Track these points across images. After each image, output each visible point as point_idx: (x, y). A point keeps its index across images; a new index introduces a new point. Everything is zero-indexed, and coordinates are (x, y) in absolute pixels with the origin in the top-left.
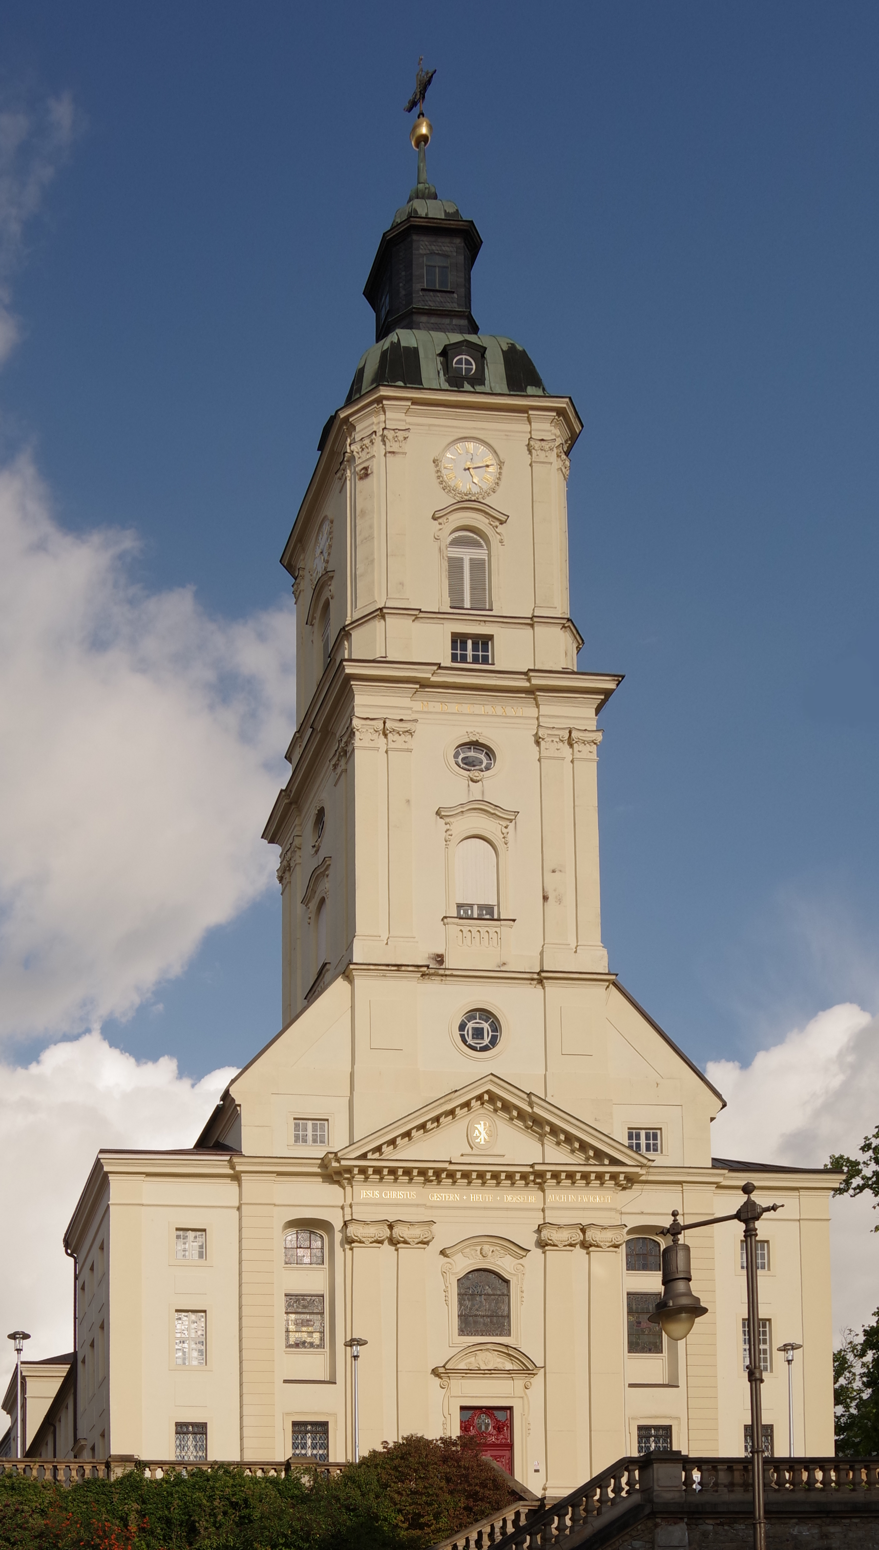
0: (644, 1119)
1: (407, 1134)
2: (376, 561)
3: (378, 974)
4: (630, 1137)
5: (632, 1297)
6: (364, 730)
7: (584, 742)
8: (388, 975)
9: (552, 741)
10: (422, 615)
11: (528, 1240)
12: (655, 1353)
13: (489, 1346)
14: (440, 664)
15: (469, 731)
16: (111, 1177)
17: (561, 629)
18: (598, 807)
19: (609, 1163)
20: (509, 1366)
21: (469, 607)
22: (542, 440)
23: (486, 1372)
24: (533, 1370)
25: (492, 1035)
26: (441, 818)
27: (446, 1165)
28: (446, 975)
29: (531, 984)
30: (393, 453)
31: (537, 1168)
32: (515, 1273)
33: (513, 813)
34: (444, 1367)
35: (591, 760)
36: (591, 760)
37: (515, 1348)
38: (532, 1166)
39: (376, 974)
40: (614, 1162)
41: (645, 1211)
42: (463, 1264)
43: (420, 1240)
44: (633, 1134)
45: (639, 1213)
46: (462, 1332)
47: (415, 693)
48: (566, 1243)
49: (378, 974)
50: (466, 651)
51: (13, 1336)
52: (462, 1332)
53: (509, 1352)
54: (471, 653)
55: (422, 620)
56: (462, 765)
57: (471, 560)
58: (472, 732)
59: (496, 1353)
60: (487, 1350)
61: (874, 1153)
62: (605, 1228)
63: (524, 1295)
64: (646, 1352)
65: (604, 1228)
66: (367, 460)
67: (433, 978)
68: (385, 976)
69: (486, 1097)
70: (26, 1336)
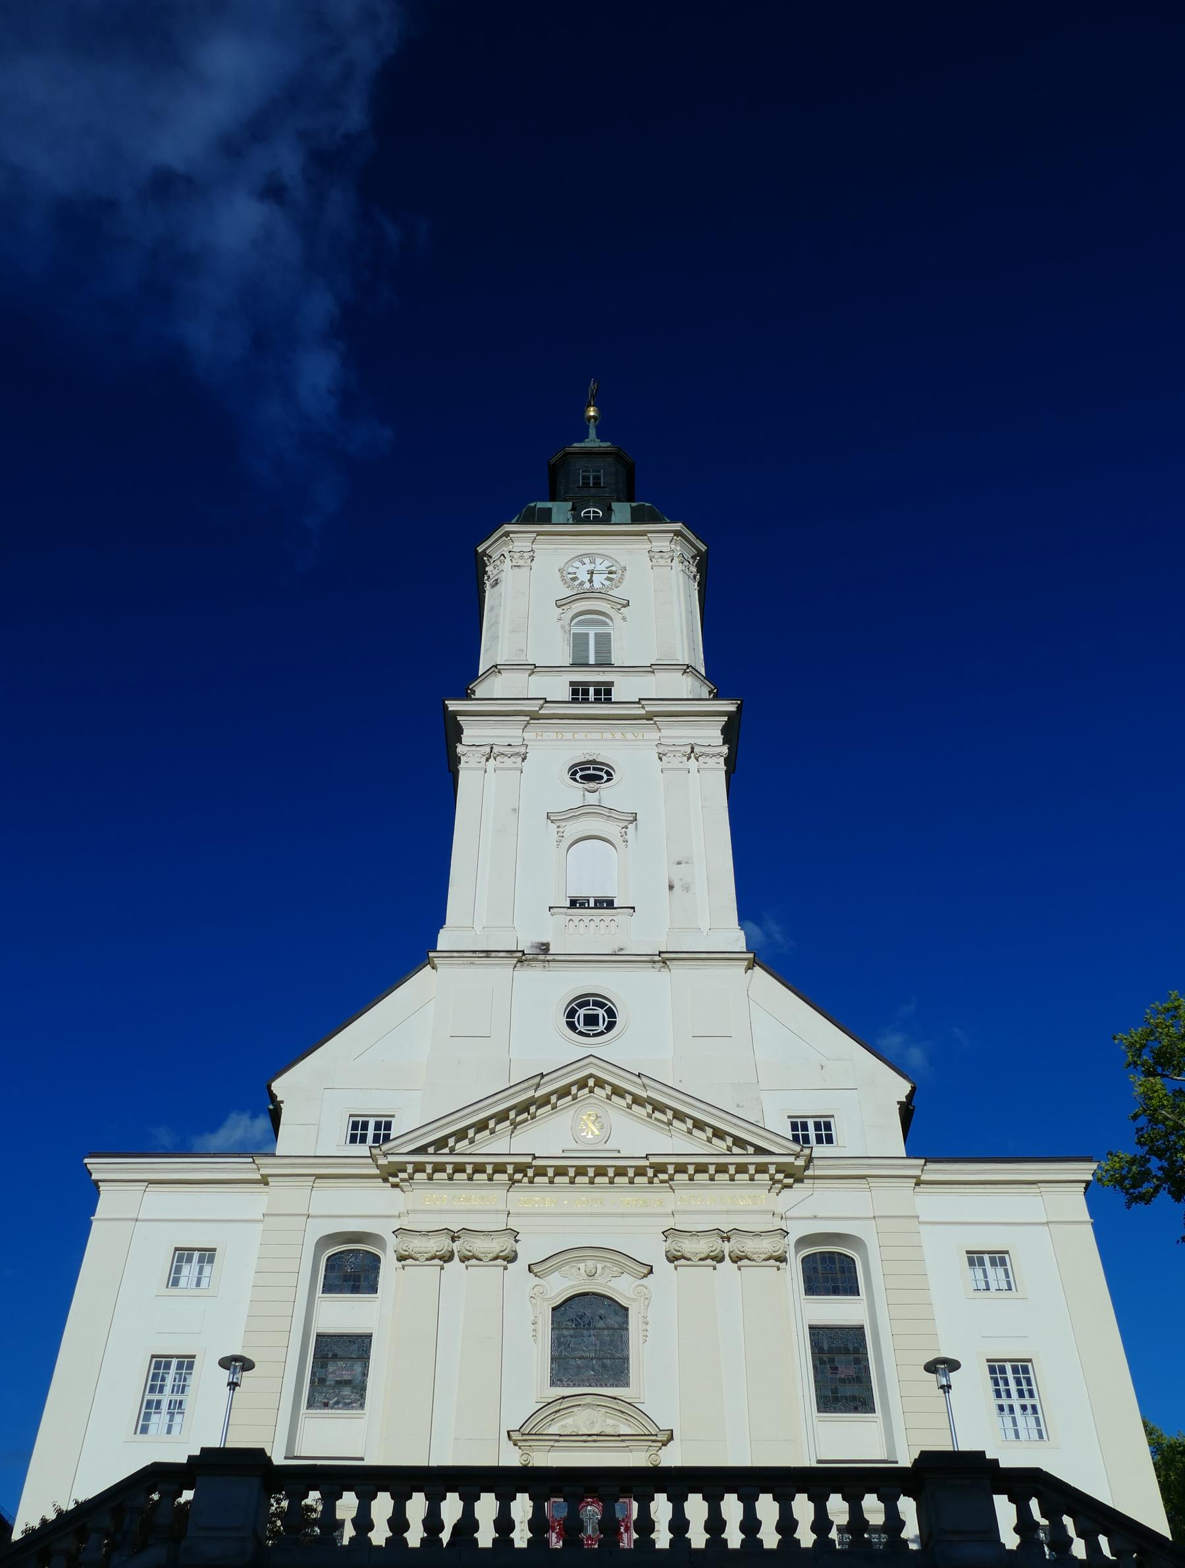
0: (810, 1106)
1: (481, 1126)
2: (500, 637)
3: (465, 962)
4: (794, 1126)
5: (821, 1333)
6: (471, 755)
7: (708, 755)
8: (476, 962)
9: (674, 756)
10: (538, 669)
11: (653, 1251)
12: (865, 1413)
13: (588, 1399)
14: (545, 699)
15: (585, 752)
16: (103, 1187)
17: (683, 674)
18: (728, 807)
19: (754, 1151)
20: (624, 1429)
21: (593, 663)
22: (661, 552)
23: (585, 1438)
24: (656, 1435)
25: (608, 1021)
26: (552, 822)
27: (529, 1159)
28: (548, 961)
29: (653, 968)
30: (519, 566)
31: (653, 1160)
32: (635, 1297)
33: (630, 815)
34: (519, 1431)
35: (719, 769)
36: (719, 769)
37: (630, 1404)
38: (647, 1157)
39: (462, 962)
40: (760, 1151)
41: (819, 1215)
42: (561, 1286)
43: (494, 1255)
44: (798, 1127)
45: (810, 1218)
46: (553, 1384)
47: (526, 726)
48: (702, 1256)
49: (465, 962)
50: (589, 696)
51: (931, 1367)
52: (553, 1384)
53: (630, 1409)
54: (593, 697)
55: (539, 674)
56: (580, 781)
57: (596, 634)
58: (588, 753)
59: (603, 1410)
60: (588, 1405)
61: (1160, 1158)
62: (756, 1235)
63: (648, 1327)
64: (850, 1412)
65: (758, 1234)
66: (497, 574)
67: (533, 965)
68: (473, 964)
69: (591, 1082)
70: (953, 1365)
